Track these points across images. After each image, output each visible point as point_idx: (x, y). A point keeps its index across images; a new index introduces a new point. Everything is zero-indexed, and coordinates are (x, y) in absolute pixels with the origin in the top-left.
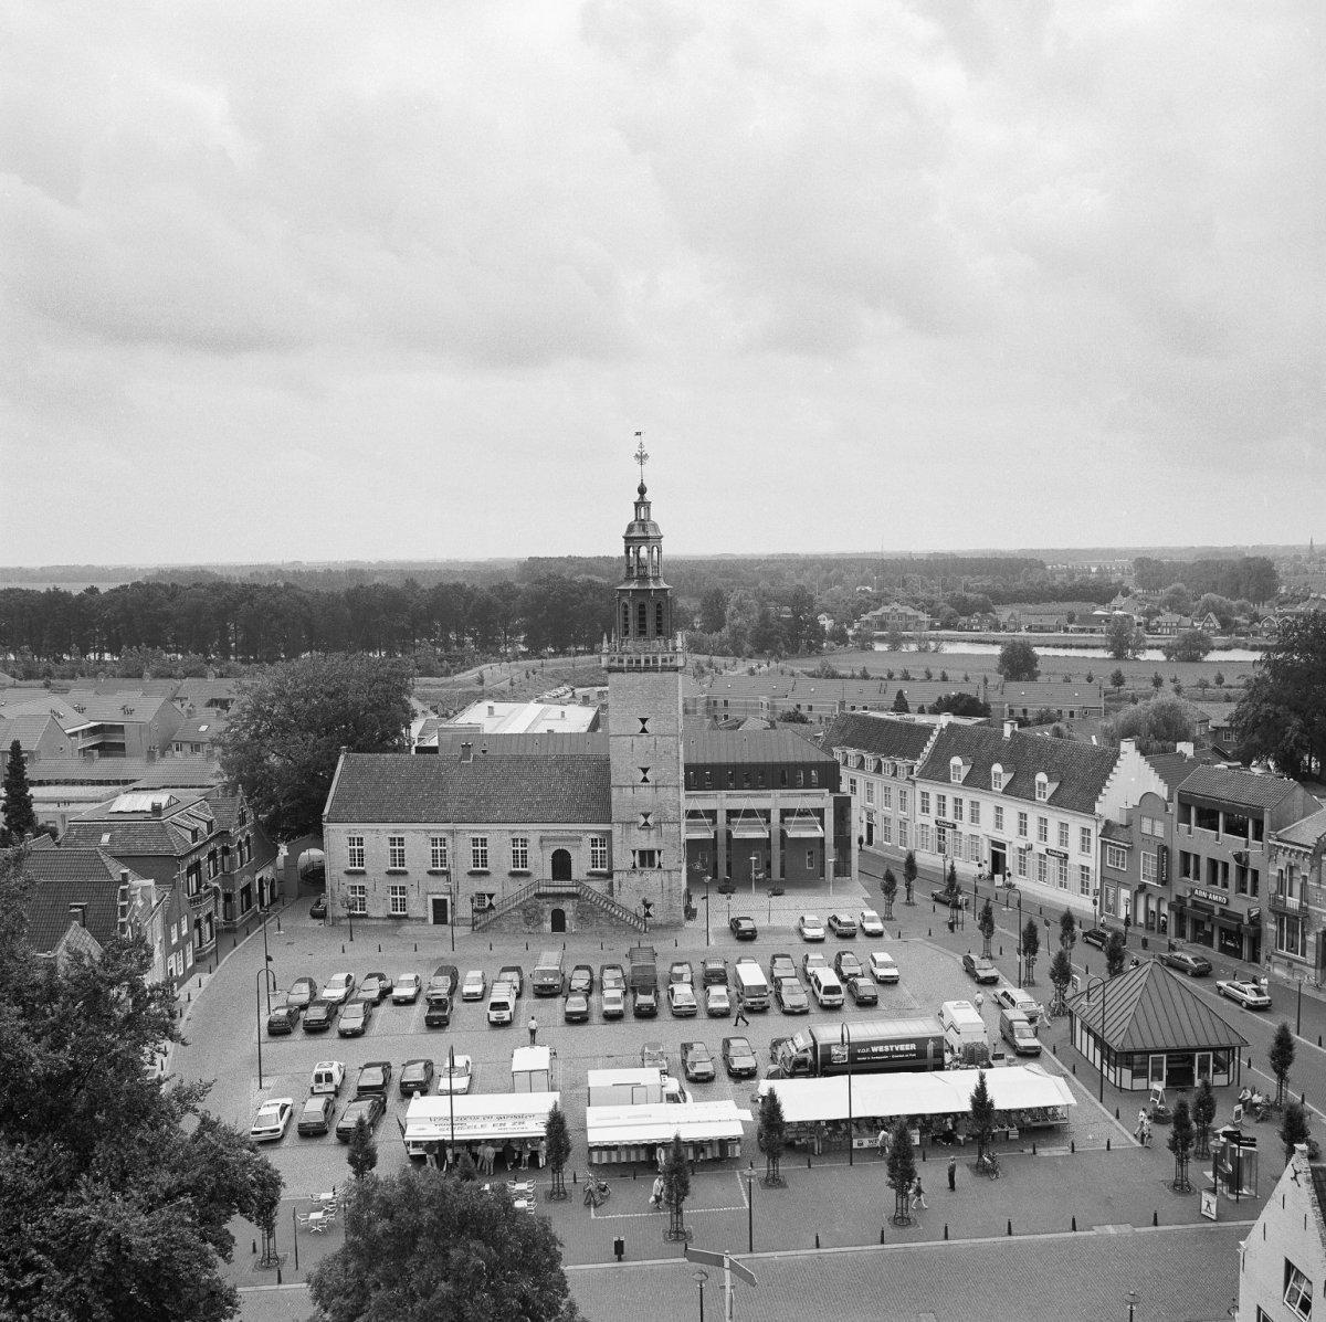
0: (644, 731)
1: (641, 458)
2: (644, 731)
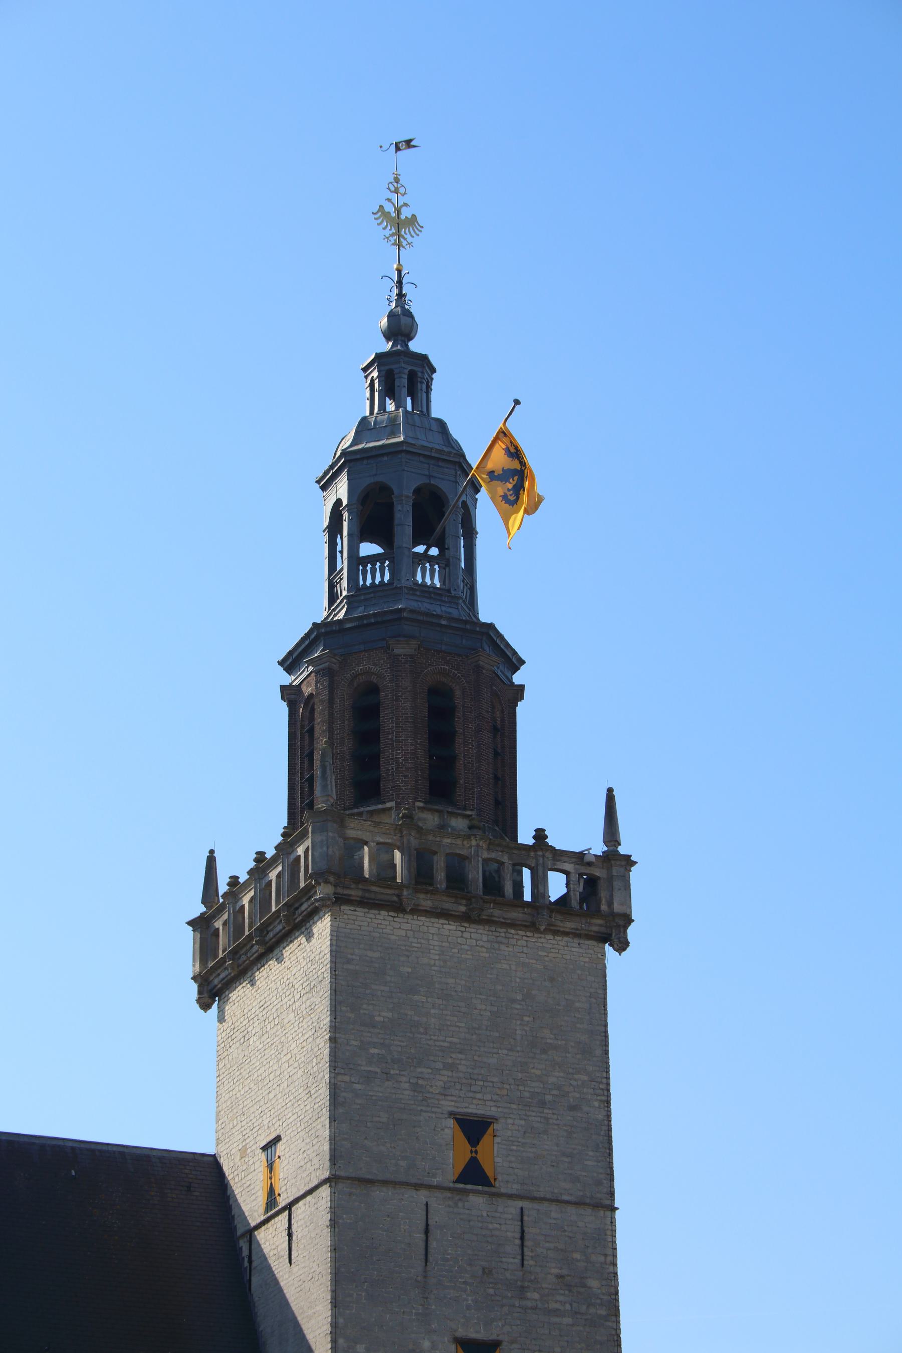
0: (474, 1175)
1: (400, 225)
2: (474, 1175)
